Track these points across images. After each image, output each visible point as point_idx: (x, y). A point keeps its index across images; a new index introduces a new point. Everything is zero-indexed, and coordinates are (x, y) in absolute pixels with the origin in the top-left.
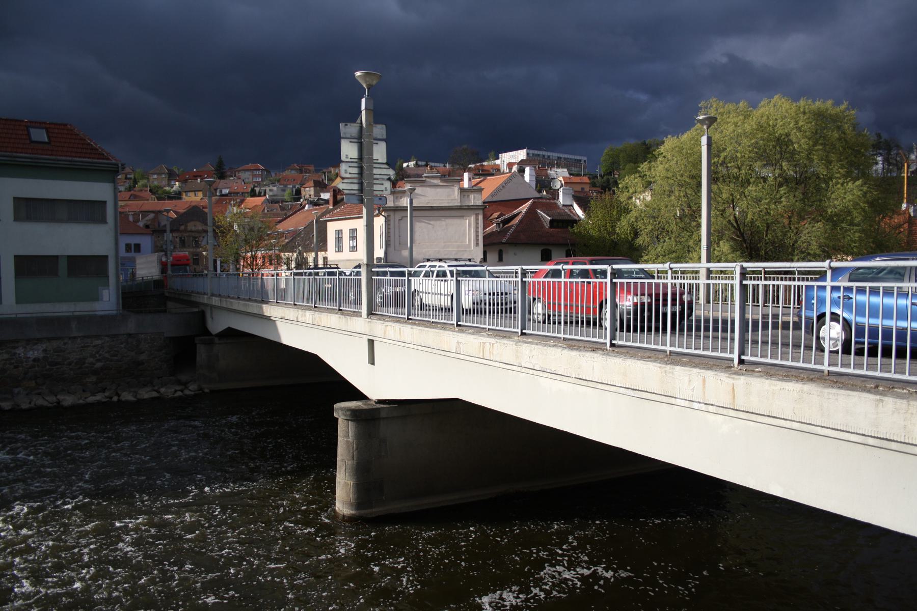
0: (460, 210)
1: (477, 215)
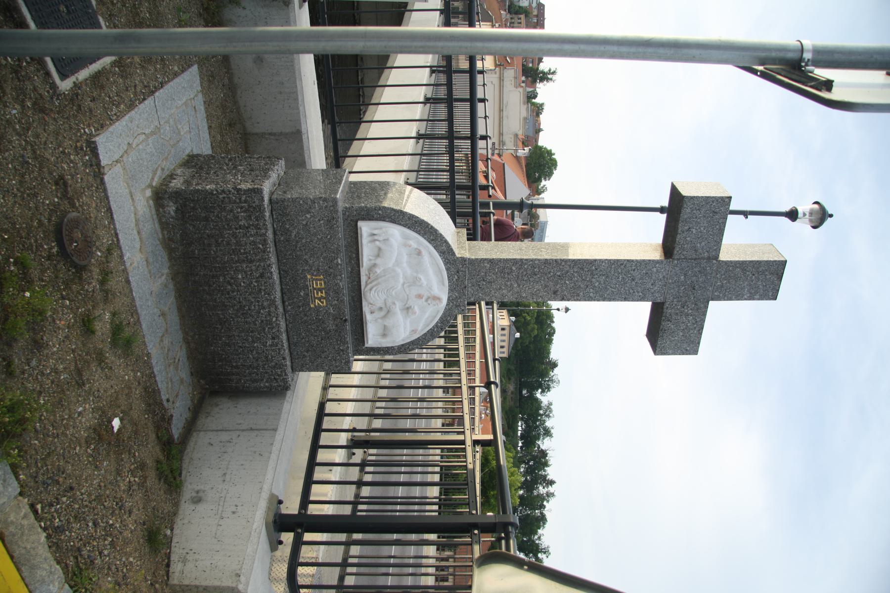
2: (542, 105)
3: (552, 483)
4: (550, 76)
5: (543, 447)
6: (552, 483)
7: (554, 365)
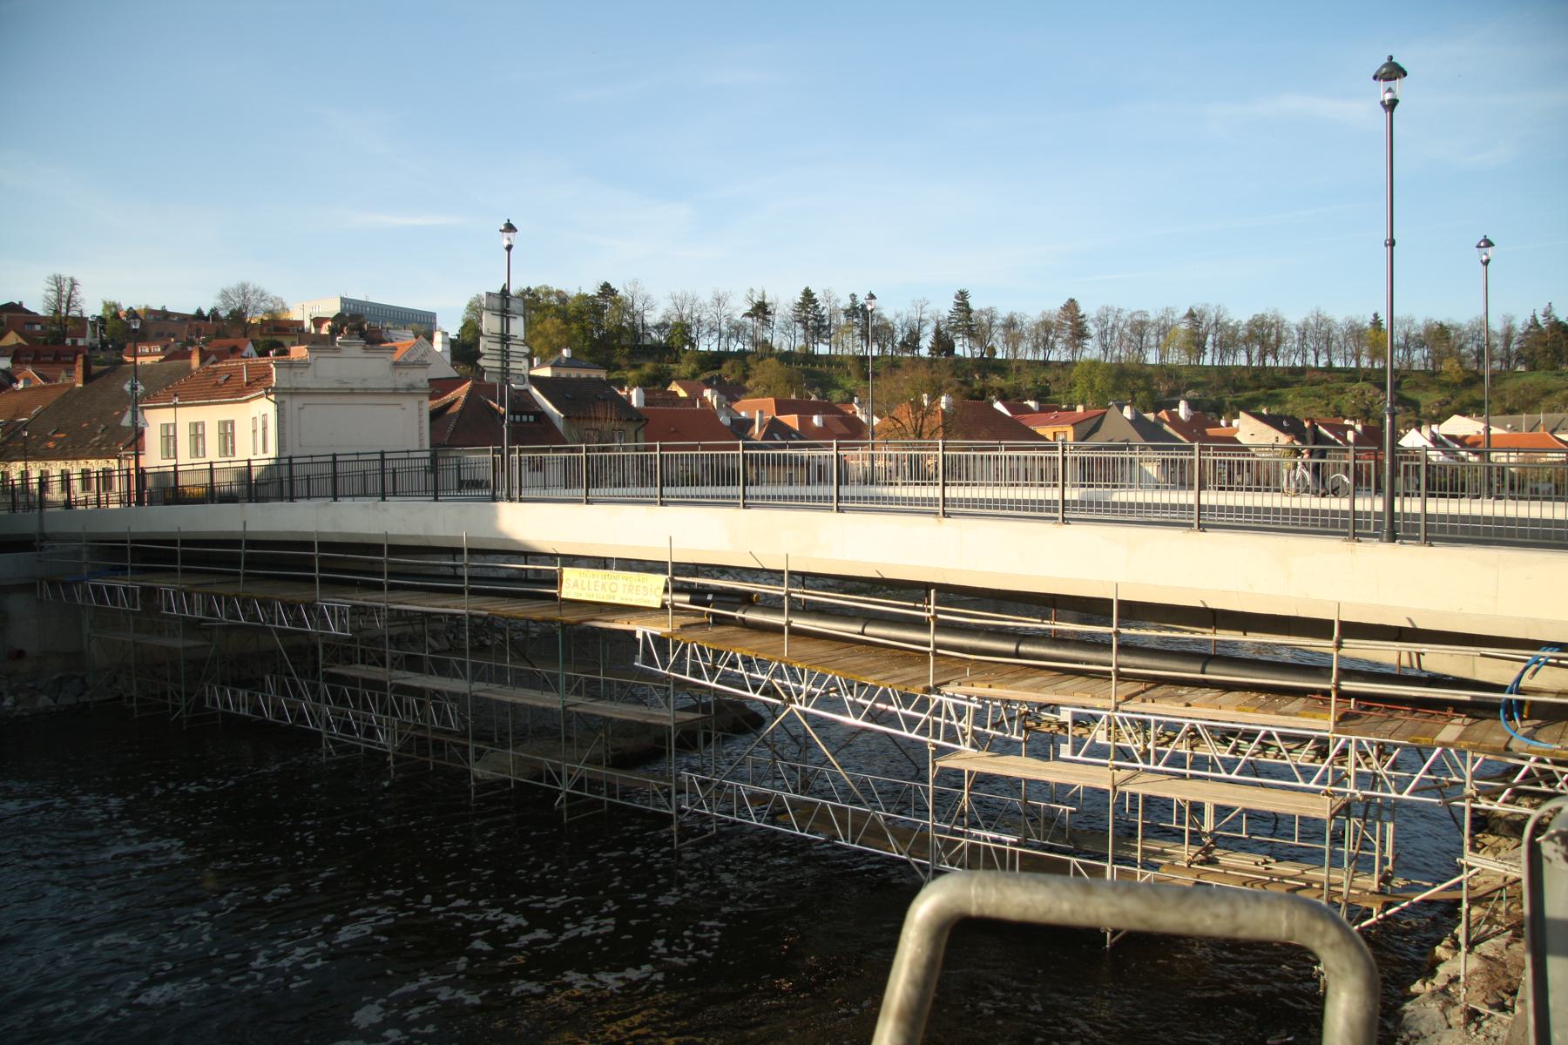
0: (410, 390)
1: (421, 402)
2: (107, 306)
3: (808, 294)
4: (66, 289)
5: (748, 308)
6: (808, 294)
7: (607, 290)
